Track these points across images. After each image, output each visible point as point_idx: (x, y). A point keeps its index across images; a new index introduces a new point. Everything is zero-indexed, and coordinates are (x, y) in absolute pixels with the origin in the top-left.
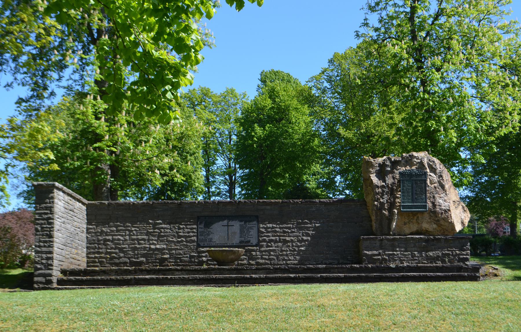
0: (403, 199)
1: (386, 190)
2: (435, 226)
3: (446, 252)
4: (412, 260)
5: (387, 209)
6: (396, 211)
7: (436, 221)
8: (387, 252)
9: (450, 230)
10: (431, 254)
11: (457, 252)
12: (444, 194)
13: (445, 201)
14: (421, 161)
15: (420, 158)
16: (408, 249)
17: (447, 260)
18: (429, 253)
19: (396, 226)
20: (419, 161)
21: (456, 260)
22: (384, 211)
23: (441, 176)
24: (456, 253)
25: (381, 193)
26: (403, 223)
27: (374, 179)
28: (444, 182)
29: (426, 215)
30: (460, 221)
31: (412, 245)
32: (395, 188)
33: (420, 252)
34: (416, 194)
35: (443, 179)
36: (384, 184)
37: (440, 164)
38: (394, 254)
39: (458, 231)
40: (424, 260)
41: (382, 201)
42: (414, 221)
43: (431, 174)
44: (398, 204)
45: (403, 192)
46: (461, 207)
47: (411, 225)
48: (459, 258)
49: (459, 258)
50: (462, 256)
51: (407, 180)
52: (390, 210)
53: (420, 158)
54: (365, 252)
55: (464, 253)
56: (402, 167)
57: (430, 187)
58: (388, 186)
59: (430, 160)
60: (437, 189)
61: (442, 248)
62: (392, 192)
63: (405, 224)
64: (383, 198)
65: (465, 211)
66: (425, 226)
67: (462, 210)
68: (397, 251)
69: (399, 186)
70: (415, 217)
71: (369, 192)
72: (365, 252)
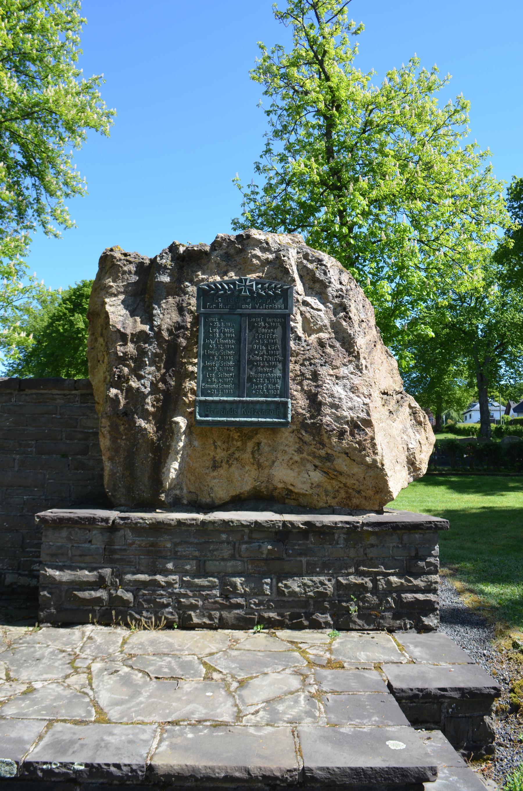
0: (205, 380)
1: (152, 348)
2: (316, 476)
3: (353, 579)
4: (223, 607)
5: (153, 414)
6: (182, 421)
7: (320, 457)
8: (129, 577)
9: (370, 493)
10: (294, 585)
11: (394, 579)
12: (351, 367)
13: (354, 389)
14: (278, 258)
15: (274, 247)
16: (211, 566)
17: (353, 608)
18: (289, 582)
19: (180, 472)
20: (271, 257)
21: (390, 609)
22: (142, 423)
23: (344, 308)
24: (389, 583)
25: (135, 360)
26: (209, 463)
27: (116, 311)
28: (351, 326)
29: (287, 438)
30: (403, 459)
31: (226, 552)
32: (183, 342)
33: (254, 577)
34: (250, 362)
35: (348, 318)
36: (146, 328)
37: (341, 272)
38: (155, 584)
39: (424, 784)
40: (269, 609)
41: (134, 384)
42: (247, 456)
43: (309, 299)
44: (191, 397)
45: (206, 357)
46: (408, 410)
47: (235, 471)
48: (399, 601)
49: (399, 601)
50: (409, 597)
51: (221, 316)
52: (163, 420)
53: (274, 247)
54: (50, 572)
55: (419, 582)
56: (212, 274)
57: (303, 341)
58: (158, 335)
59: (306, 256)
60: (329, 350)
61: (333, 567)
62: (172, 356)
63: (215, 466)
64: (140, 378)
65: (420, 423)
66: (284, 475)
67: (409, 422)
68: (165, 572)
69: (193, 339)
70: (250, 445)
71: (100, 358)
72: (50, 572)
